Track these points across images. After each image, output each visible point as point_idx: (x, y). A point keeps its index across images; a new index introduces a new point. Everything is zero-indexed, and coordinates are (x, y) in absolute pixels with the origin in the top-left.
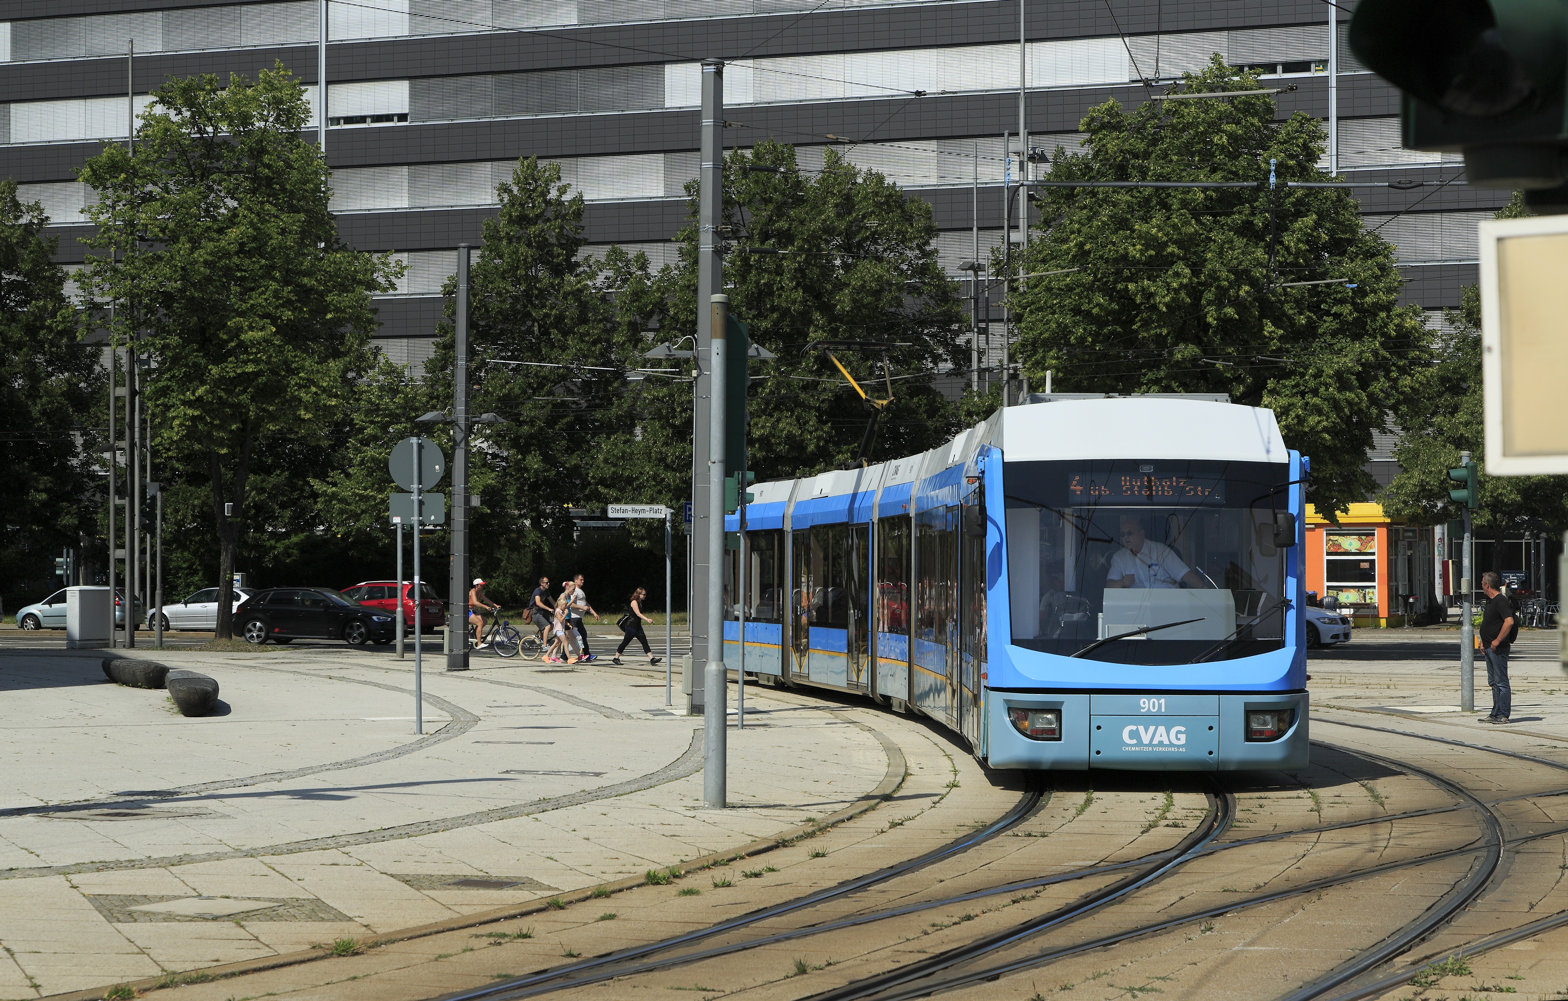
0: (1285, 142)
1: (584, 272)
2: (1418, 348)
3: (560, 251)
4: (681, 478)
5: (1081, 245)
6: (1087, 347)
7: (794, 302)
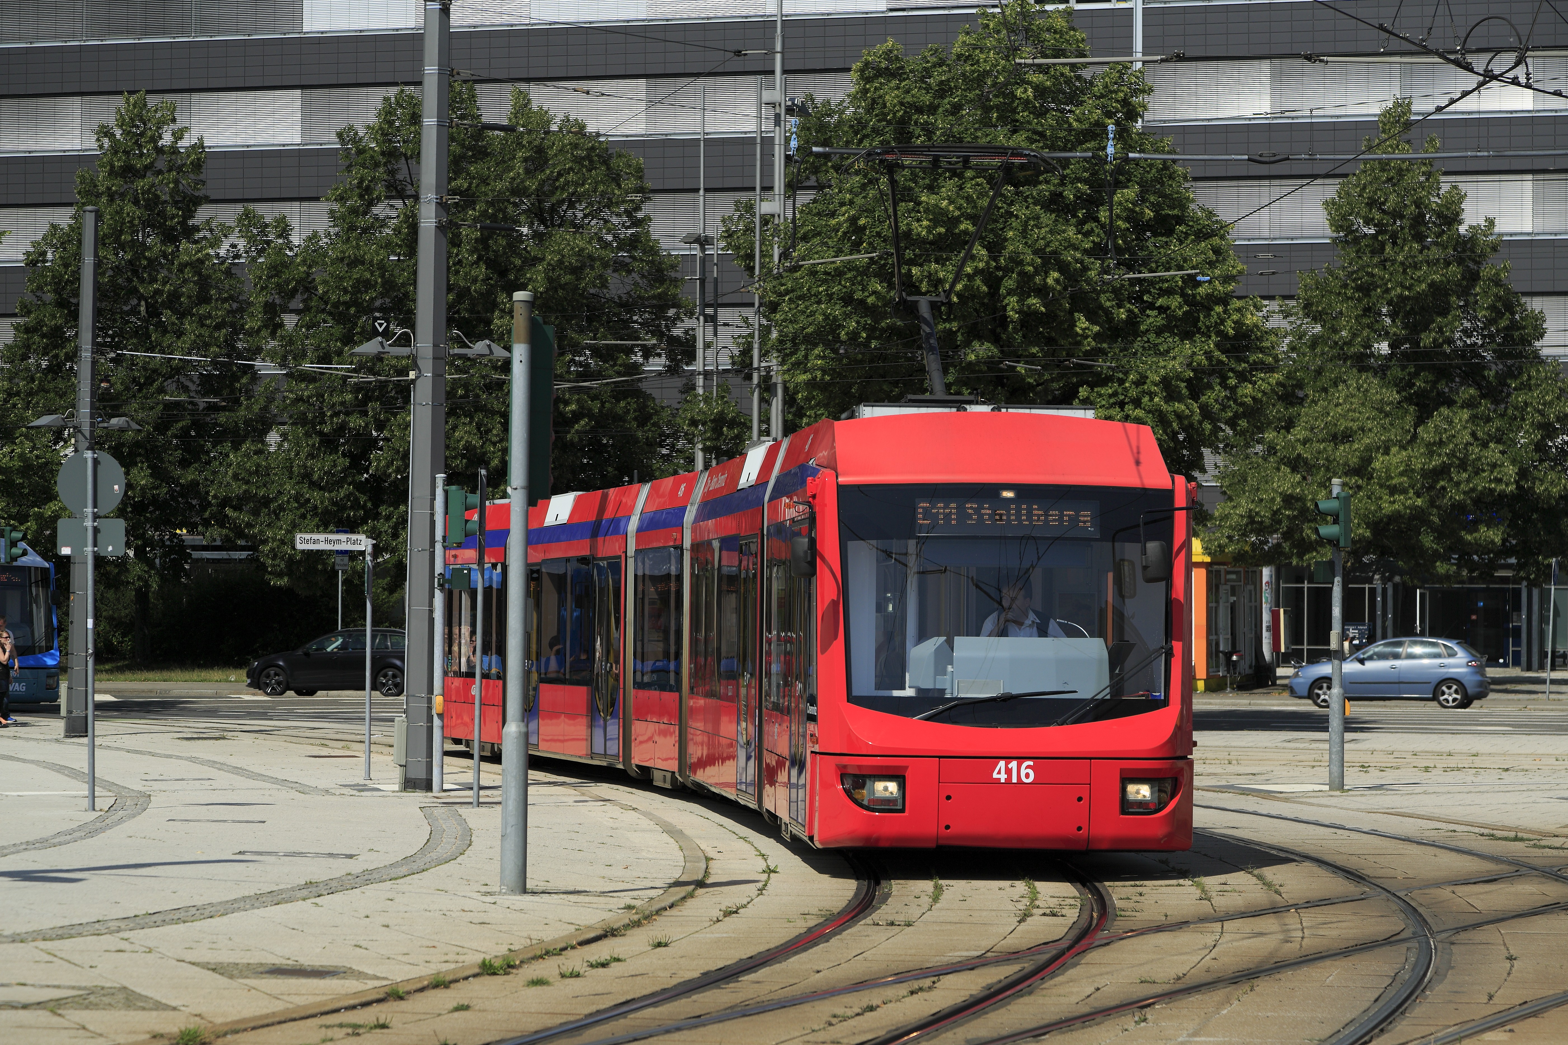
0: (1102, 96)
1: (205, 238)
2: (1262, 350)
3: (175, 211)
4: (331, 499)
5: (853, 220)
6: (861, 344)
7: (475, 280)
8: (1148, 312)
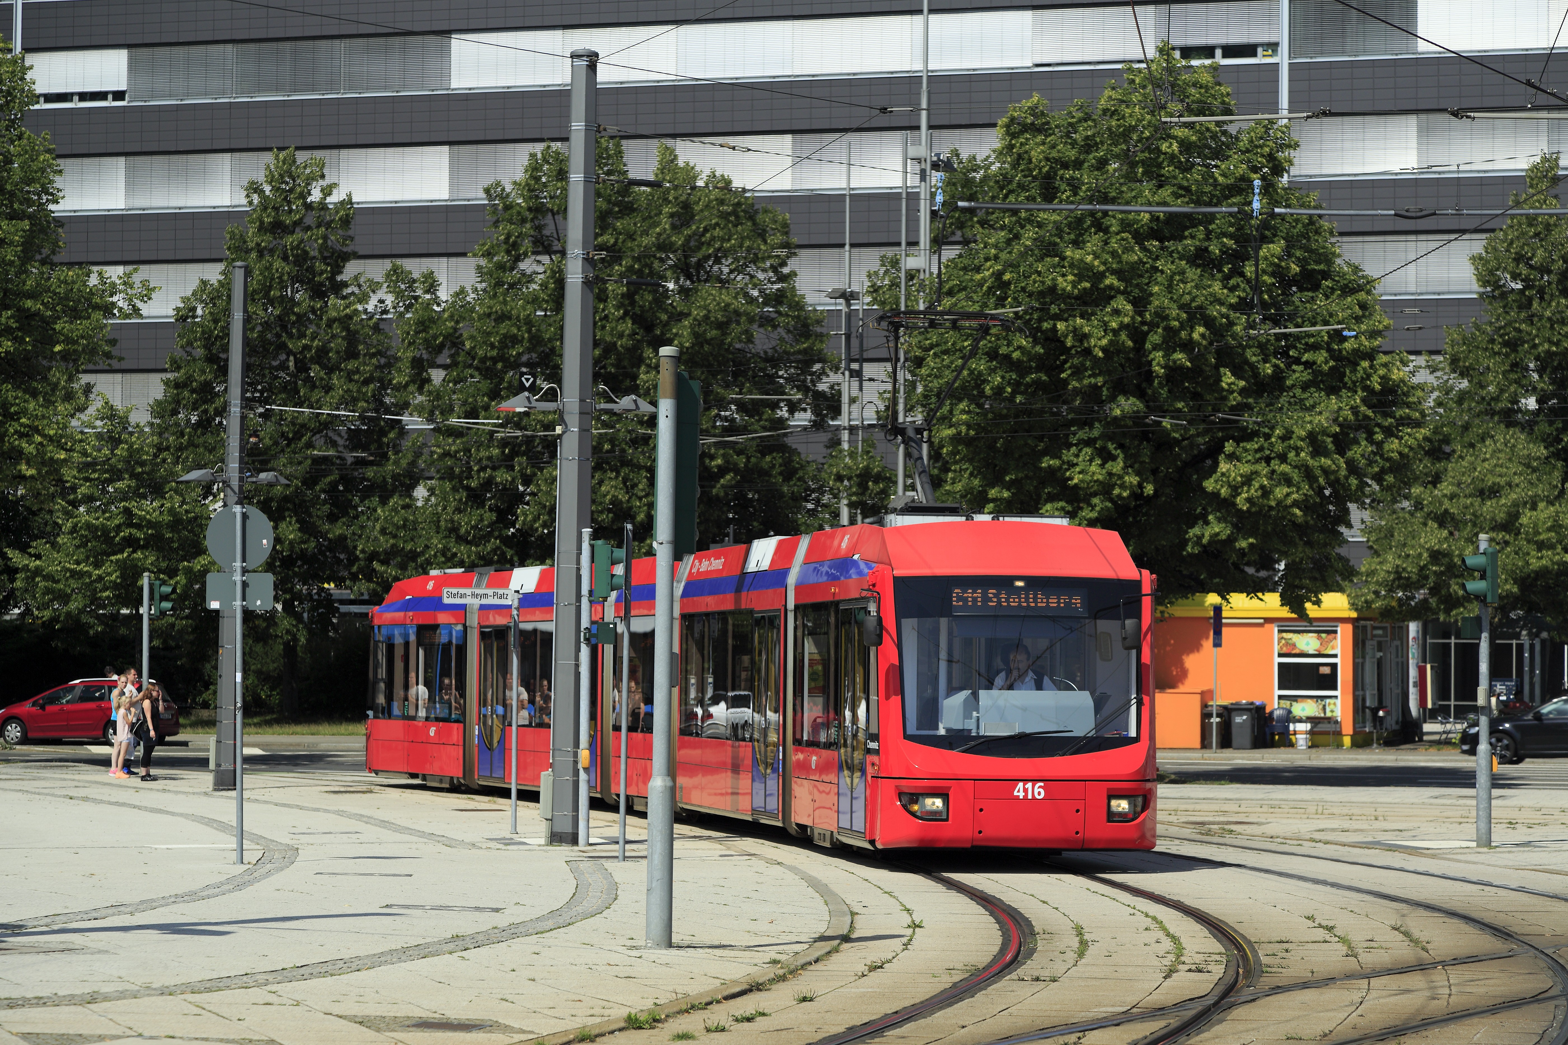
0: (1248, 151)
1: (353, 293)
5: (998, 275)
6: (1006, 398)
7: (621, 336)
8: (1294, 367)
